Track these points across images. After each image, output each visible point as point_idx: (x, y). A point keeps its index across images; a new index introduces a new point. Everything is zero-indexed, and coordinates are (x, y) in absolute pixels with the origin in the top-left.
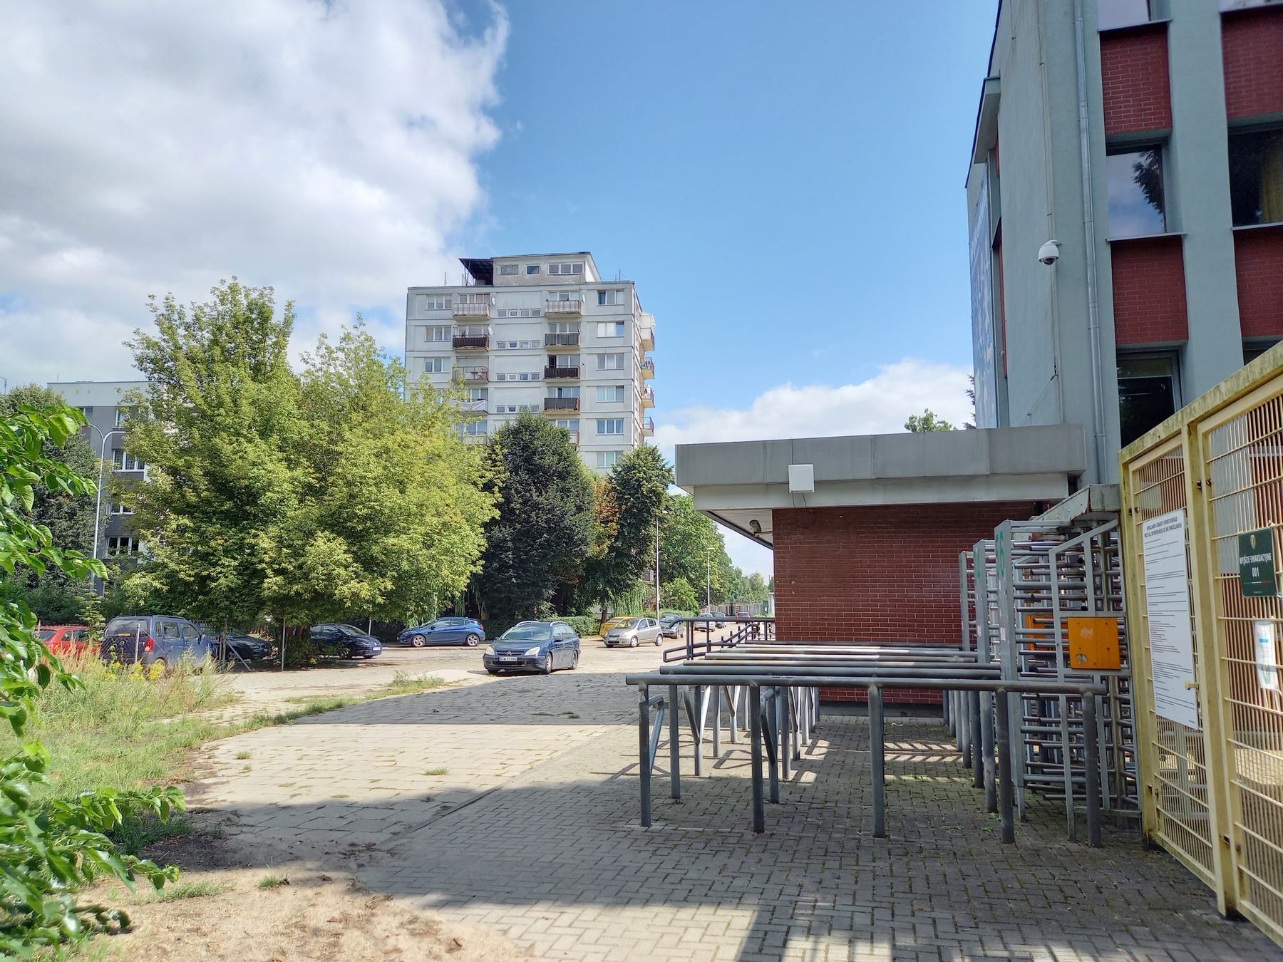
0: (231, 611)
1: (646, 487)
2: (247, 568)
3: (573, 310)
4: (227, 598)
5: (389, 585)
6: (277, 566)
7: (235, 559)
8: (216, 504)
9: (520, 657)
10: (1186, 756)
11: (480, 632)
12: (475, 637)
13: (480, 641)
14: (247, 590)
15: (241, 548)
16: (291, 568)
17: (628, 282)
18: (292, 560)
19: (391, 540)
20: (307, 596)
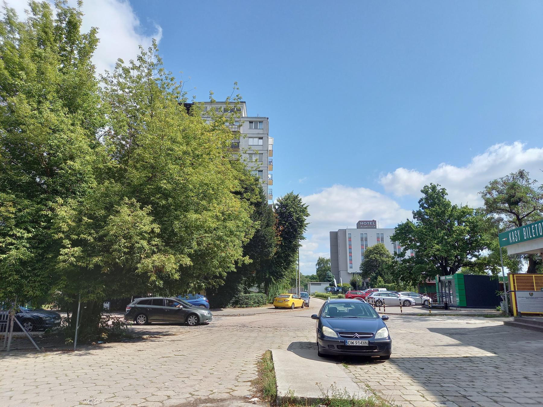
0: (21, 286)
1: (295, 216)
2: (41, 242)
3: (236, 130)
4: (18, 272)
5: (187, 261)
6: (76, 237)
7: (29, 232)
8: (11, 173)
10: (73, 301)
11: (206, 303)
14: (41, 264)
15: (35, 220)
16: (90, 239)
17: (265, 118)
18: (93, 231)
19: (192, 216)
20: (106, 270)
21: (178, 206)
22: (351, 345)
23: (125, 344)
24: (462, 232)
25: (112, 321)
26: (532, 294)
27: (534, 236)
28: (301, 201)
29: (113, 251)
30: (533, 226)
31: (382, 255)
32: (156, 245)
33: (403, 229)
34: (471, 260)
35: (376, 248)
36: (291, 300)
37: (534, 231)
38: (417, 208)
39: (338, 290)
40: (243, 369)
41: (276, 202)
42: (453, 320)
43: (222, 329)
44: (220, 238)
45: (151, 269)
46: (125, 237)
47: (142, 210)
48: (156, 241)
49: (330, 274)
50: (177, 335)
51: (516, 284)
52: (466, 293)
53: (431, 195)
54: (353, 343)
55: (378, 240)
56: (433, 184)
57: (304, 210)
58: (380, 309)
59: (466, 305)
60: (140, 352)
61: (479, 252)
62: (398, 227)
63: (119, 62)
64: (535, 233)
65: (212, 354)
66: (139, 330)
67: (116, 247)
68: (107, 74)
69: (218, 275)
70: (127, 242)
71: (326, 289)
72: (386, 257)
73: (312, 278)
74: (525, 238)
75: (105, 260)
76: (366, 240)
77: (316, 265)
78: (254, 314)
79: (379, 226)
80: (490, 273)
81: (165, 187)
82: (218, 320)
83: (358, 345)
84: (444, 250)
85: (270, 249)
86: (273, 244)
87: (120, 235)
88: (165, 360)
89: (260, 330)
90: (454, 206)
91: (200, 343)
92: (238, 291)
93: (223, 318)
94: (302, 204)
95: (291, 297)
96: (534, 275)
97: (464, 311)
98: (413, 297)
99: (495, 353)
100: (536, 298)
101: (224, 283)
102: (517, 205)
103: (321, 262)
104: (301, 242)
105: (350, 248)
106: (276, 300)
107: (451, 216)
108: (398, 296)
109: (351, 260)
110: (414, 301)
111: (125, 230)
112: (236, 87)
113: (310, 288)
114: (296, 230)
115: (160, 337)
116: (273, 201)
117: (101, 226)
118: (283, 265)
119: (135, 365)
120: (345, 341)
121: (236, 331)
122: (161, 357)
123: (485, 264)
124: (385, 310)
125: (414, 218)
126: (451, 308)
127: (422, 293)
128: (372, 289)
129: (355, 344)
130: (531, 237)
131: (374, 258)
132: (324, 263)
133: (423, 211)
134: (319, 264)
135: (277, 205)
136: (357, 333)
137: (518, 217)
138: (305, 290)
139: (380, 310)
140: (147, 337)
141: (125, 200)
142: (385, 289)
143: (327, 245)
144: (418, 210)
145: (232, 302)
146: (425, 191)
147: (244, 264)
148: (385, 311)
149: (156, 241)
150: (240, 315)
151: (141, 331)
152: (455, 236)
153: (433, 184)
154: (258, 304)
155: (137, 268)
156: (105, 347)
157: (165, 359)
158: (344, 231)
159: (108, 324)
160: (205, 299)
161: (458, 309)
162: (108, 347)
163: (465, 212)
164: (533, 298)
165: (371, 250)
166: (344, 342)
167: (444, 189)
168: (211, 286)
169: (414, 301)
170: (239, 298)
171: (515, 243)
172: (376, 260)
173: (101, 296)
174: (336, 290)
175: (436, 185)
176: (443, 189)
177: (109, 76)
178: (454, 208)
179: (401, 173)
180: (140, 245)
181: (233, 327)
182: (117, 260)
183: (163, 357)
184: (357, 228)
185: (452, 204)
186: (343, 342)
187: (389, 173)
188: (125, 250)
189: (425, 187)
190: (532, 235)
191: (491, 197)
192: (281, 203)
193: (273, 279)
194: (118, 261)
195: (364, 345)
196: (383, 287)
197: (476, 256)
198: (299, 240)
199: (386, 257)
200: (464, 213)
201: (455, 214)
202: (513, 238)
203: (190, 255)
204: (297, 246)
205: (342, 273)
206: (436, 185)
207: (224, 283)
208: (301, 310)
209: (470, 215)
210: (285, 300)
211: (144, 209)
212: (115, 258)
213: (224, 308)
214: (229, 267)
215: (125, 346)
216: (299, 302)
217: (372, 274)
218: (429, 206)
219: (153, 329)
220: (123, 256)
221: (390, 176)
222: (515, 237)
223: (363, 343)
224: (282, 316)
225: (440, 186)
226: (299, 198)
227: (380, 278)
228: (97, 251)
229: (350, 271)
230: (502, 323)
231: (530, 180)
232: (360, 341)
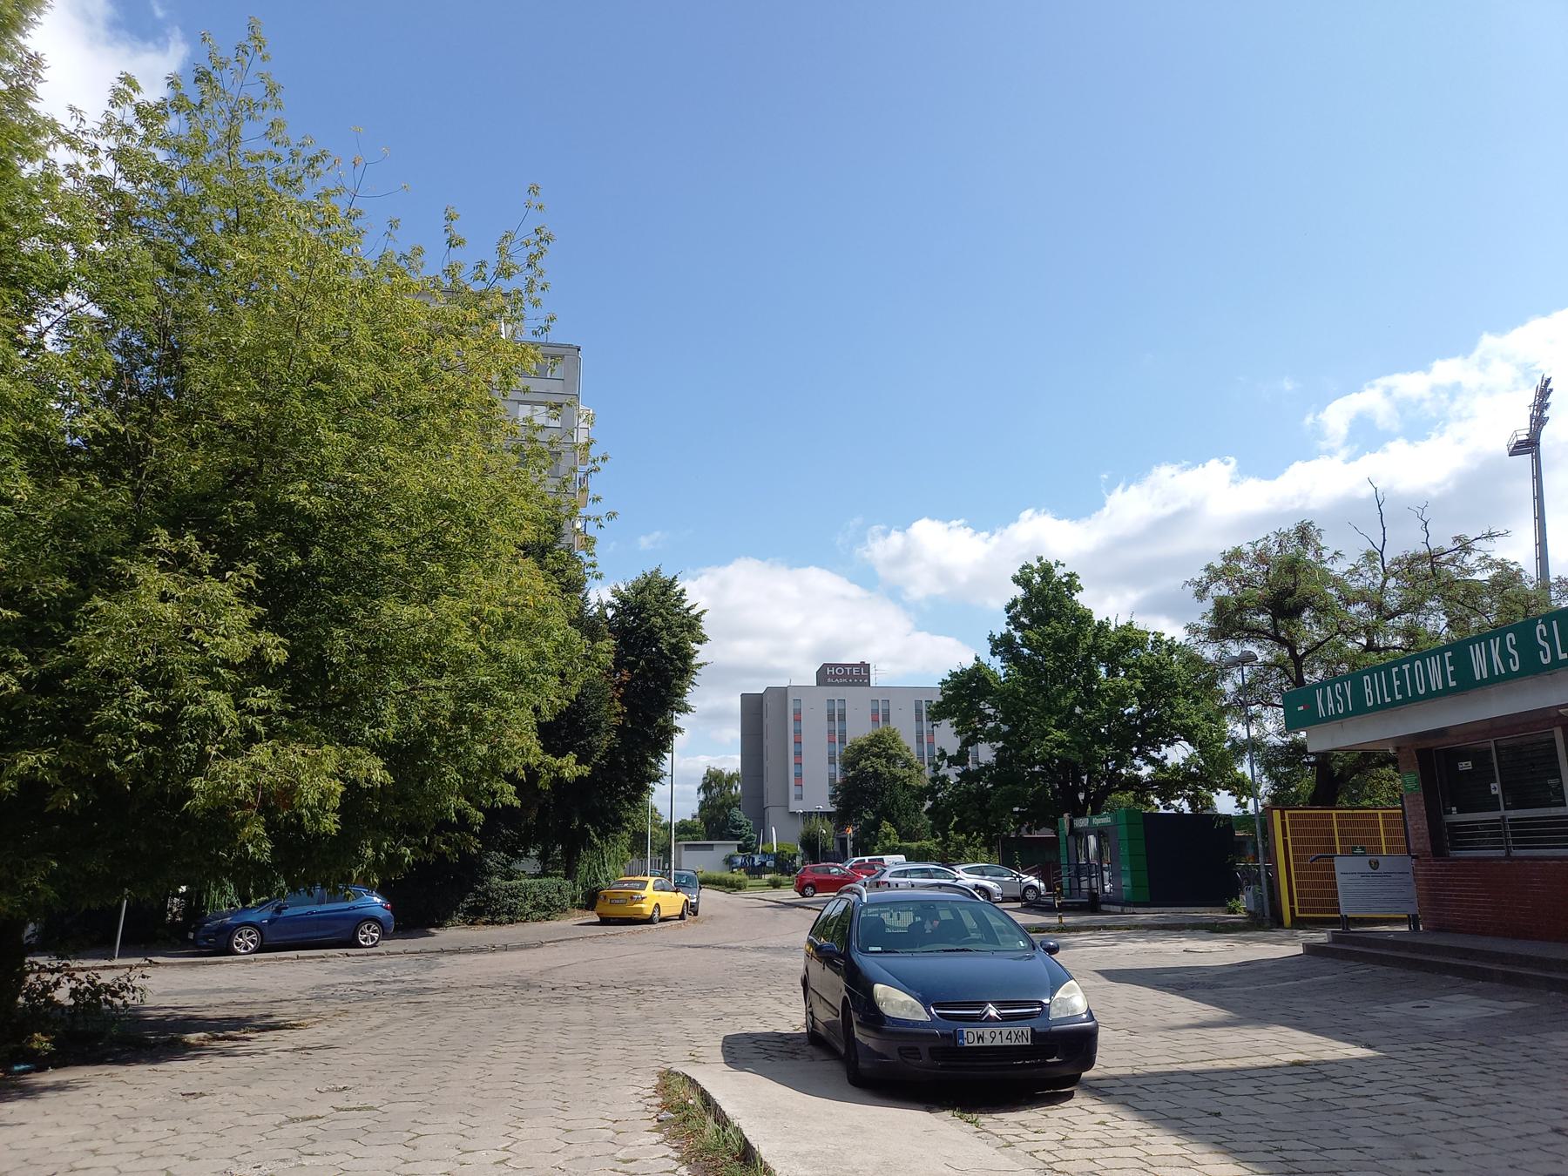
5: (376, 771)
9: (1037, 1024)
12: (374, 927)
13: (385, 935)
17: (569, 347)
18: (18, 656)
21: (342, 579)
22: (975, 1044)
23: (124, 1068)
24: (1121, 698)
25: (68, 986)
26: (1377, 863)
27: (1399, 697)
28: (683, 597)
29: (98, 729)
30: (1395, 670)
31: (891, 759)
32: (261, 711)
33: (962, 683)
34: (1140, 773)
35: (877, 740)
36: (654, 896)
37: (1398, 683)
38: (1001, 627)
39: (763, 864)
40: (619, 1155)
41: (607, 597)
42: (1133, 942)
43: (457, 999)
44: (481, 694)
45: (246, 797)
46: (146, 678)
47: (223, 580)
48: (263, 698)
49: (739, 815)
50: (306, 1027)
51: (1289, 838)
53: (1040, 591)
54: (981, 1038)
55: (875, 720)
56: (1044, 561)
57: (692, 626)
60: (192, 1101)
61: (1159, 750)
62: (949, 679)
63: (121, 86)
64: (1402, 689)
65: (473, 1095)
66: (162, 1013)
67: (110, 713)
68: (75, 122)
69: (454, 819)
70: (152, 698)
71: (729, 861)
72: (902, 768)
73: (684, 829)
74: (1369, 704)
75: (65, 763)
76: (842, 718)
77: (699, 790)
78: (541, 945)
80: (1186, 808)
81: (303, 502)
82: (429, 968)
83: (997, 1042)
85: (595, 740)
86: (603, 725)
87: (127, 670)
88: (311, 1131)
89: (589, 998)
90: (1101, 623)
91: (406, 1053)
92: (486, 873)
93: (444, 959)
94: (686, 605)
95: (650, 885)
96: (1334, 812)
97: (1144, 916)
98: (994, 878)
99: (1369, 1047)
100: (1388, 874)
101: (480, 846)
102: (1299, 616)
103: (713, 782)
104: (680, 720)
105: (798, 742)
106: (605, 897)
107: (1094, 649)
108: (957, 876)
109: (799, 776)
110: (999, 890)
111: (145, 654)
112: (535, 201)
114: (667, 684)
115: (249, 1035)
116: (600, 595)
117: (51, 636)
118: (623, 788)
119: (191, 1159)
120: (955, 1031)
121: (509, 1004)
122: (284, 1118)
123: (1177, 782)
125: (993, 653)
126: (1104, 907)
127: (1008, 862)
128: (867, 859)
129: (987, 1043)
130: (1388, 700)
131: (871, 770)
132: (720, 786)
133: (1018, 635)
134: (706, 787)
135: (611, 605)
136: (992, 1003)
137: (1292, 651)
138: (664, 865)
140: (198, 1039)
141: (157, 540)
142: (902, 858)
143: (732, 734)
144: (1004, 632)
145: (465, 906)
146: (1022, 580)
147: (558, 782)
149: (263, 698)
150: (494, 949)
151: (167, 1016)
152: (1104, 706)
153: (1044, 561)
154: (548, 910)
155: (189, 794)
156: (46, 1089)
157: (305, 1129)
158: (782, 693)
159: (53, 997)
160: (377, 900)
161: (1127, 909)
162: (58, 1087)
163: (1129, 639)
164: (1380, 875)
165: (861, 748)
166: (954, 1036)
167: (1074, 574)
168: (431, 858)
169: (999, 890)
171: (1337, 716)
172: (877, 775)
173: (42, 899)
174: (757, 862)
175: (1054, 565)
176: (1071, 575)
177: (84, 127)
178: (1102, 627)
179: (929, 535)
180: (202, 710)
181: (494, 991)
182: (112, 764)
183: (292, 1120)
184: (818, 684)
185: (1098, 617)
186: (948, 1036)
187: (893, 531)
188: (144, 726)
189: (1024, 567)
190: (1391, 694)
191: (1231, 592)
192: (624, 601)
194: (116, 767)
195: (1017, 1043)
197: (1151, 761)
198: (675, 714)
199: (902, 768)
200: (1126, 643)
201: (1106, 645)
202: (1331, 705)
203: (382, 749)
204: (668, 732)
205: (773, 814)
206: (1054, 565)
207: (480, 846)
208: (679, 927)
209: (1142, 649)
210: (632, 898)
211: (228, 574)
212: (106, 756)
213: (438, 926)
214: (493, 794)
215: (125, 1079)
216: (672, 902)
217: (864, 814)
218: (1033, 621)
219: (210, 1006)
220: (137, 751)
221: (896, 539)
222: (1336, 701)
223: (1014, 1037)
224: (623, 947)
225: (1064, 565)
226: (677, 589)
227: (886, 827)
228: (31, 729)
229: (798, 807)
230: (1299, 950)
231: (1324, 552)
232: (1005, 1031)
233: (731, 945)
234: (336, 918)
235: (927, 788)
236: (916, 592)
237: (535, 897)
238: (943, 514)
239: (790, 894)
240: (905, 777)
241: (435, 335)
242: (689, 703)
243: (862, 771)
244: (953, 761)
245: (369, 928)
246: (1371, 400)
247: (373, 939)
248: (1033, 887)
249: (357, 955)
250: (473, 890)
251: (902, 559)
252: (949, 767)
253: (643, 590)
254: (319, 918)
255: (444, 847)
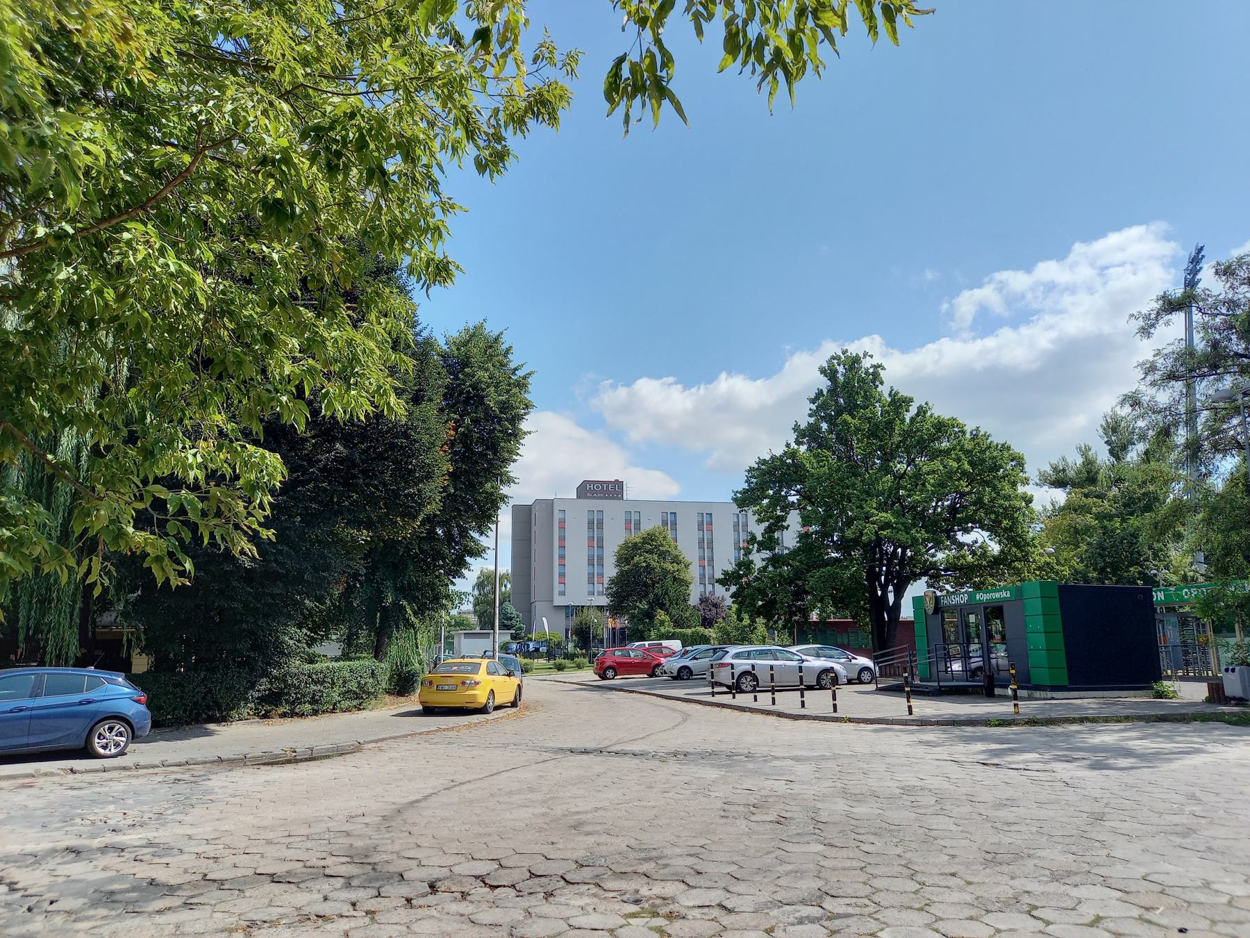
12: (119, 727)
13: (135, 737)
31: (663, 555)
38: (805, 421)
39: (537, 650)
52: (1066, 645)
55: (628, 528)
58: (773, 699)
59: (1065, 682)
76: (601, 523)
79: (630, 493)
82: (185, 804)
84: (902, 524)
94: (512, 366)
95: (483, 669)
106: (431, 683)
109: (562, 575)
113: (460, 645)
114: (494, 448)
124: (803, 703)
139: (803, 705)
145: (256, 695)
148: (835, 711)
154: (359, 697)
158: (550, 504)
161: (1037, 694)
170: (285, 681)
172: (649, 569)
174: (531, 649)
175: (861, 356)
184: (578, 497)
193: (409, 611)
196: (668, 638)
205: (539, 607)
206: (861, 356)
210: (463, 683)
216: (504, 688)
221: (622, 392)
225: (871, 356)
227: (661, 615)
229: (559, 601)
233: (628, 748)
234: (48, 717)
235: (733, 573)
236: (635, 436)
237: (345, 682)
238: (655, 375)
239: (589, 675)
240: (674, 571)
241: (218, 59)
242: (511, 474)
243: (636, 565)
244: (763, 546)
245: (111, 729)
246: (986, 294)
247: (117, 745)
248: (867, 669)
249: (87, 771)
250: (265, 674)
251: (627, 408)
252: (758, 551)
253: (465, 344)
254: (31, 717)
255: (140, 537)
